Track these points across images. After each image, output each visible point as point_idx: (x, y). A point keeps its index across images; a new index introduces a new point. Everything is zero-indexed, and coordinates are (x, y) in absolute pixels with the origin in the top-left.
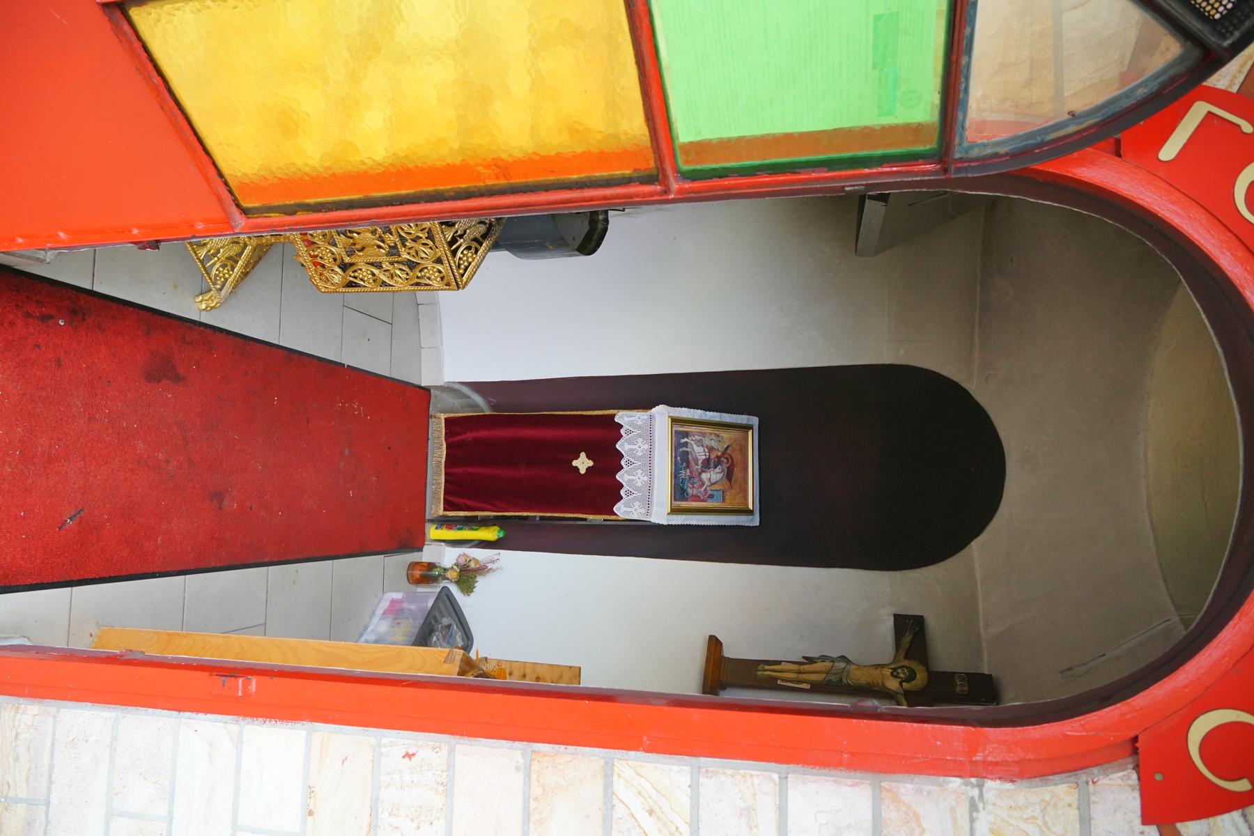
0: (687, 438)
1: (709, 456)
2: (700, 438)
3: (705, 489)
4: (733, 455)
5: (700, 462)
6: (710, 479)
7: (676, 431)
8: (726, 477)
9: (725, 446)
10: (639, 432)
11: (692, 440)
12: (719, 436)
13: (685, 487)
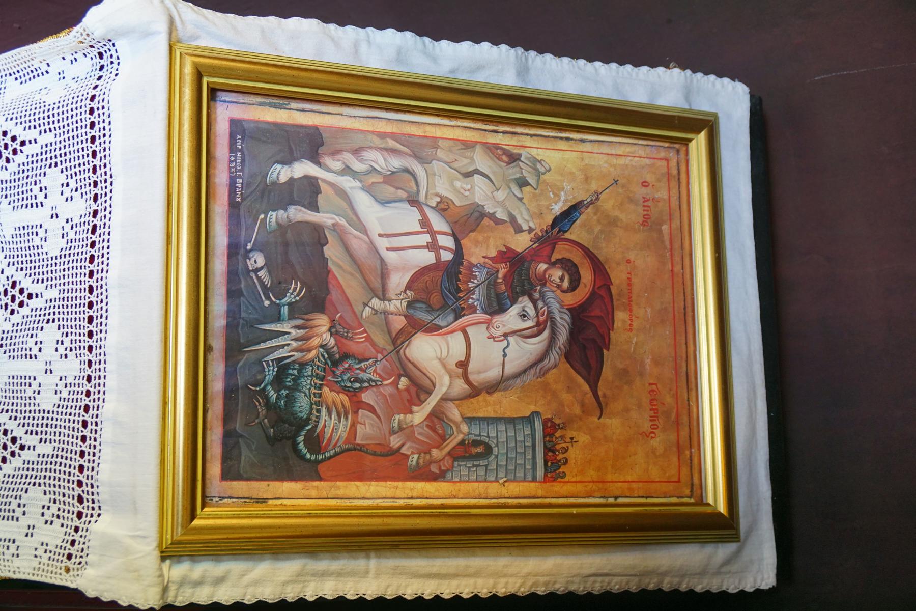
0: (315, 158)
1: (459, 252)
2: (396, 163)
3: (436, 416)
4: (604, 251)
5: (398, 281)
6: (463, 365)
7: (235, 123)
8: (568, 356)
9: (558, 208)
10: (49, 138)
11: (347, 171)
12: (513, 159)
13: (302, 404)
